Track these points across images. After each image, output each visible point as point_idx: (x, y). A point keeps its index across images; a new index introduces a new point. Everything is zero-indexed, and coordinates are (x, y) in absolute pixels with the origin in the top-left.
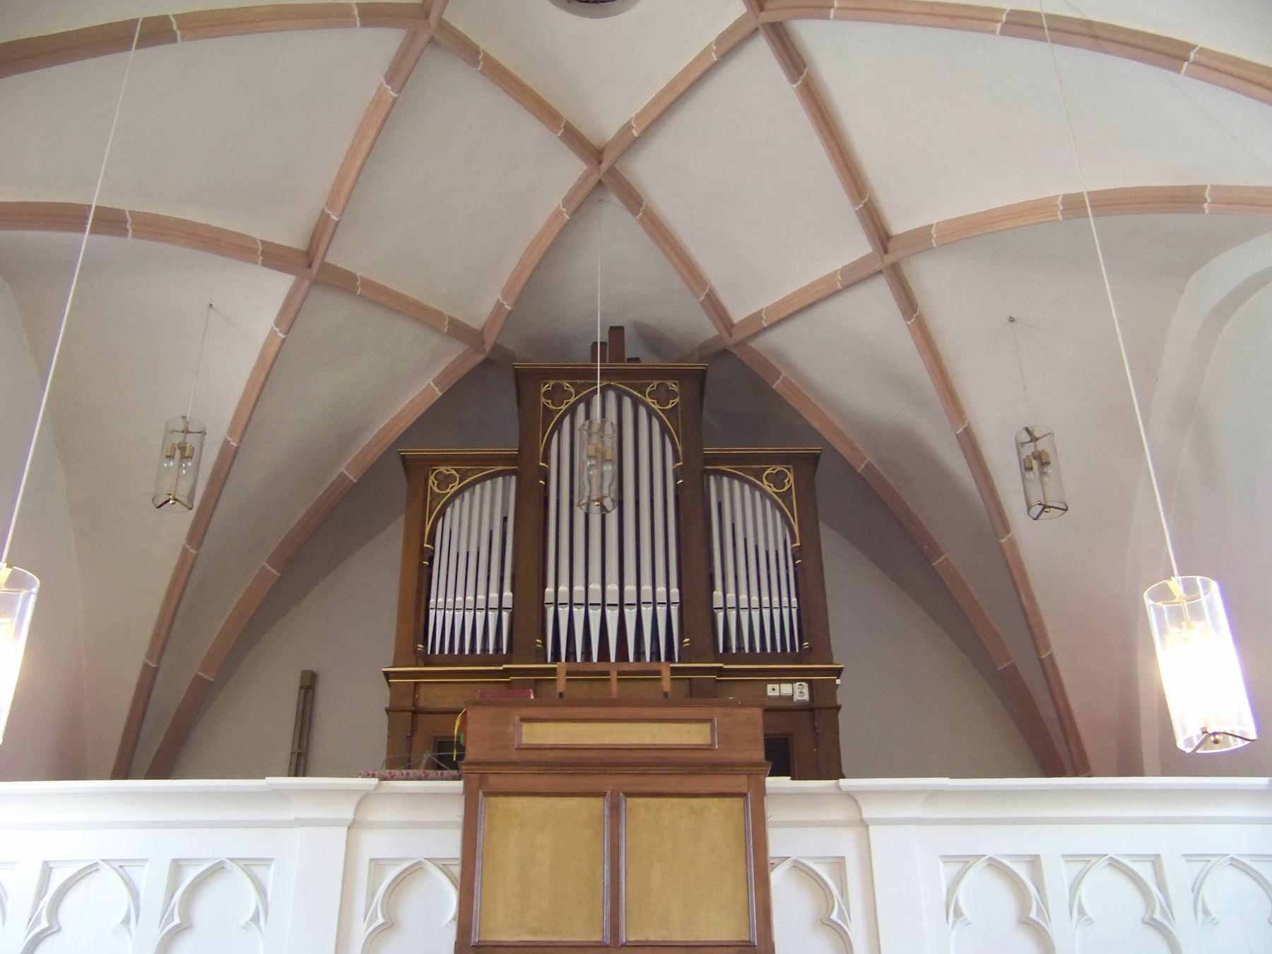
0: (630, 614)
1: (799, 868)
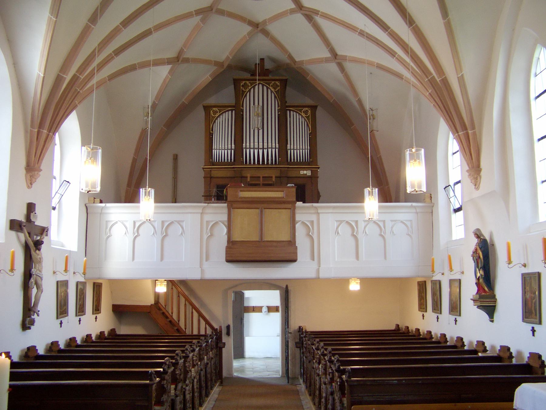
0: (265, 151)
1: (303, 223)
